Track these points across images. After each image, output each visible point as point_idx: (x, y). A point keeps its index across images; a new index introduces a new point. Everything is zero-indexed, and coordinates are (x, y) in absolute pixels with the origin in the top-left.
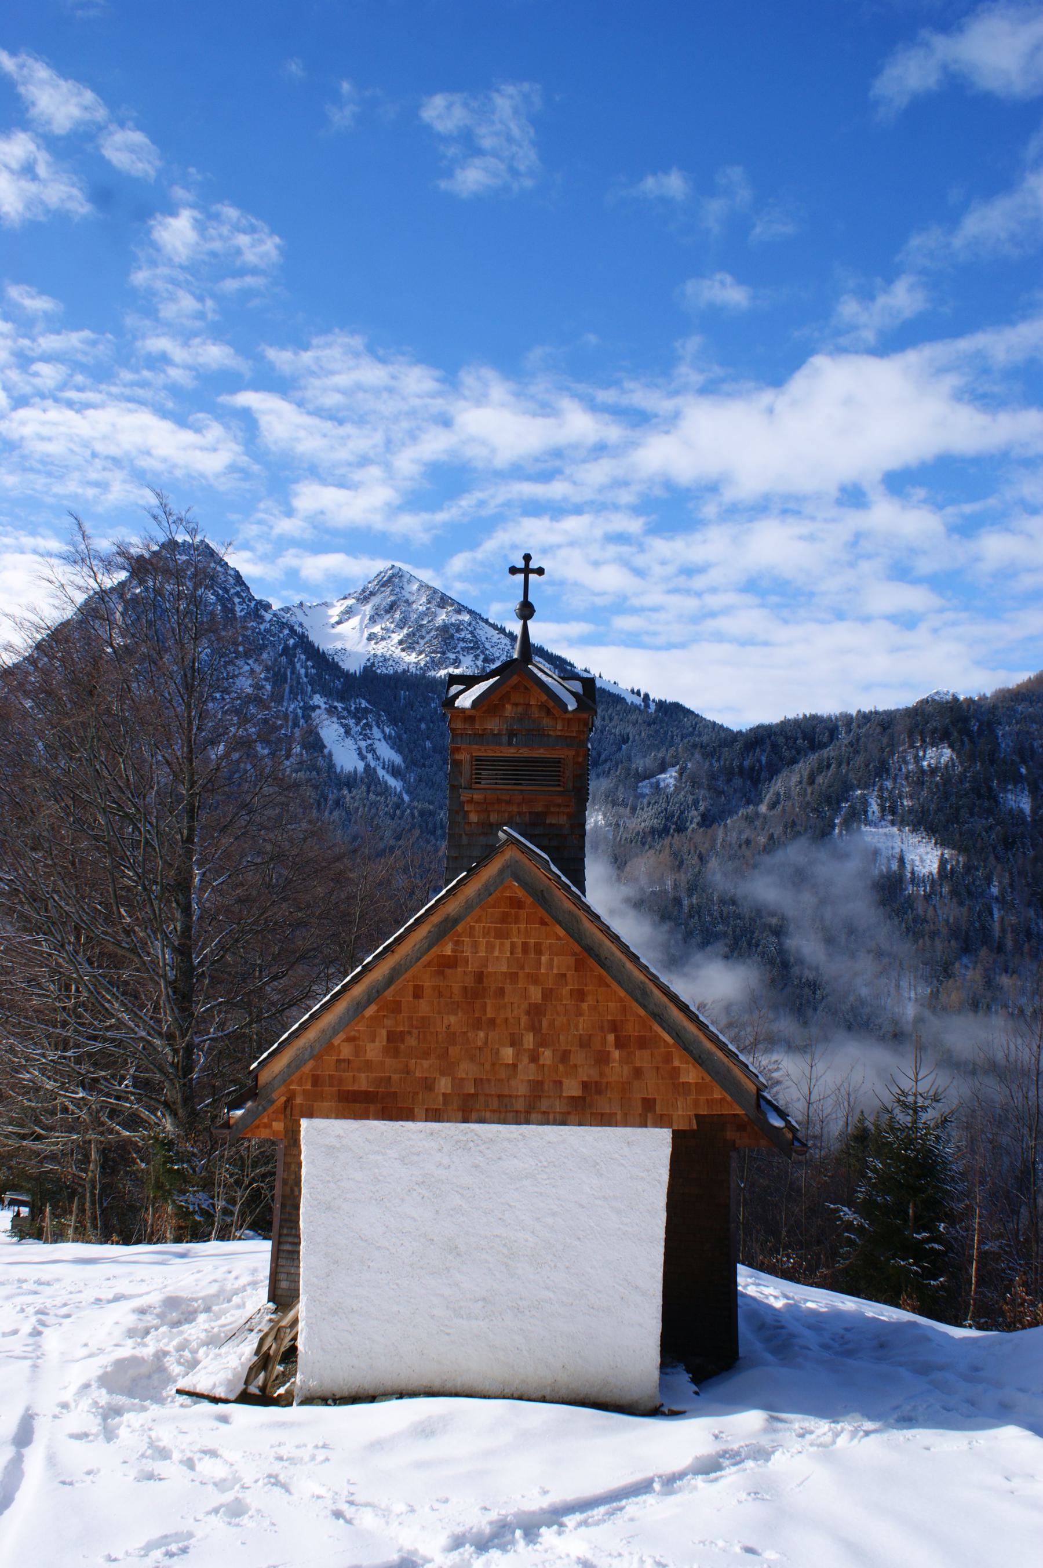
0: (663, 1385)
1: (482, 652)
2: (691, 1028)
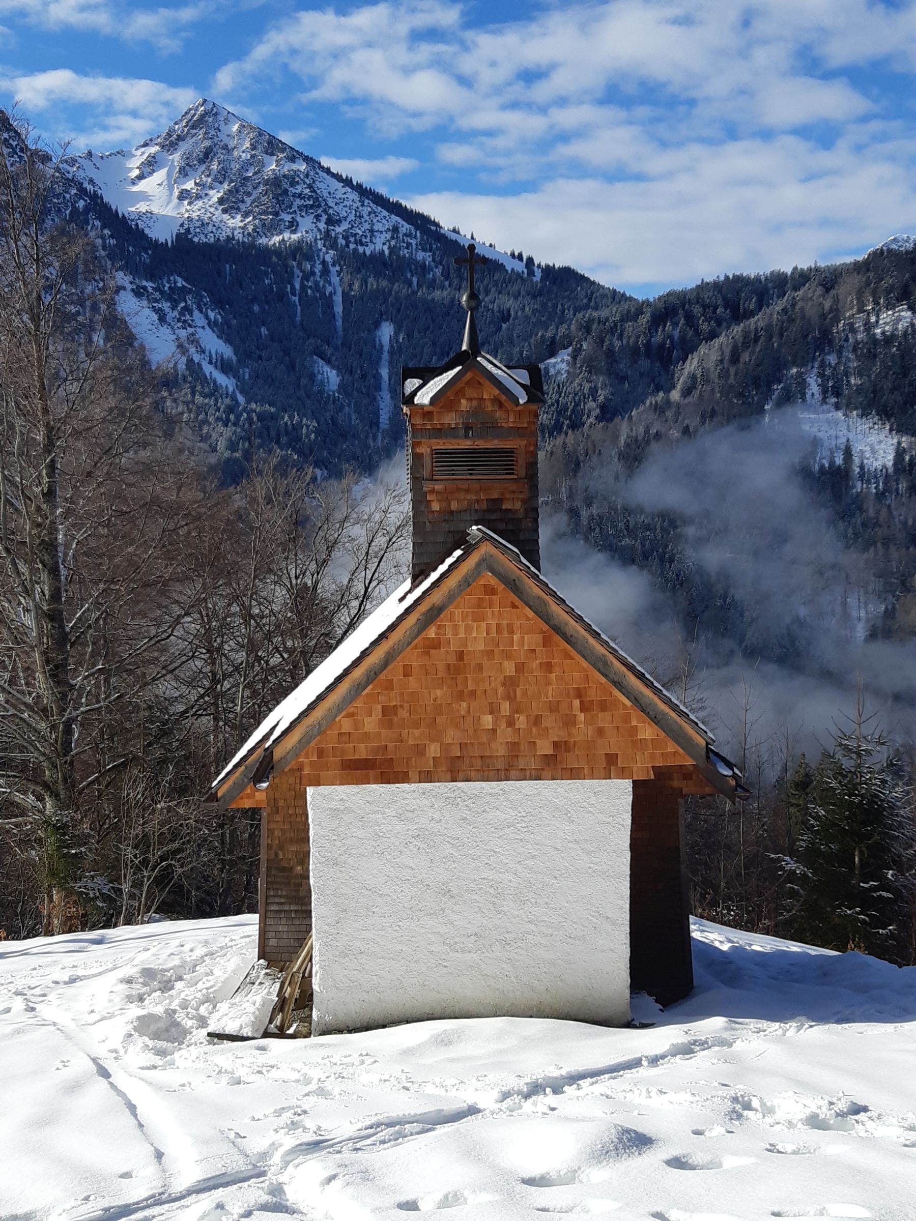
0: (632, 1005)
1: (325, 211)
2: (647, 692)
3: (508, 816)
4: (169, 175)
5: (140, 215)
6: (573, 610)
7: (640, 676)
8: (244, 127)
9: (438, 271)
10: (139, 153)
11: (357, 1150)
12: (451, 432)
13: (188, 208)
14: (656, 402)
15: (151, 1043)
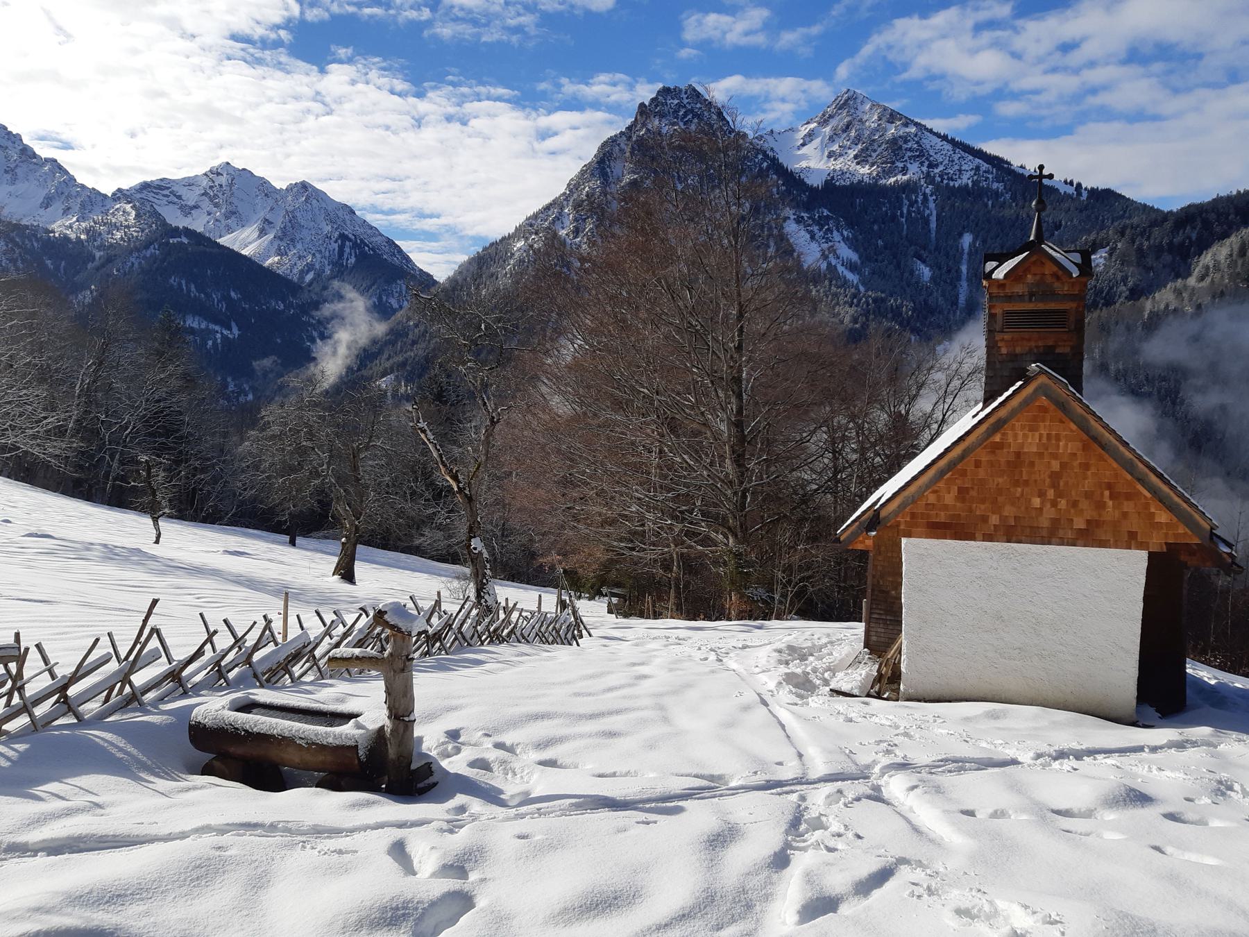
0: (1137, 711)
4: (822, 142)
5: (802, 170)
7: (1160, 476)
9: (1008, 196)
12: (1020, 298)
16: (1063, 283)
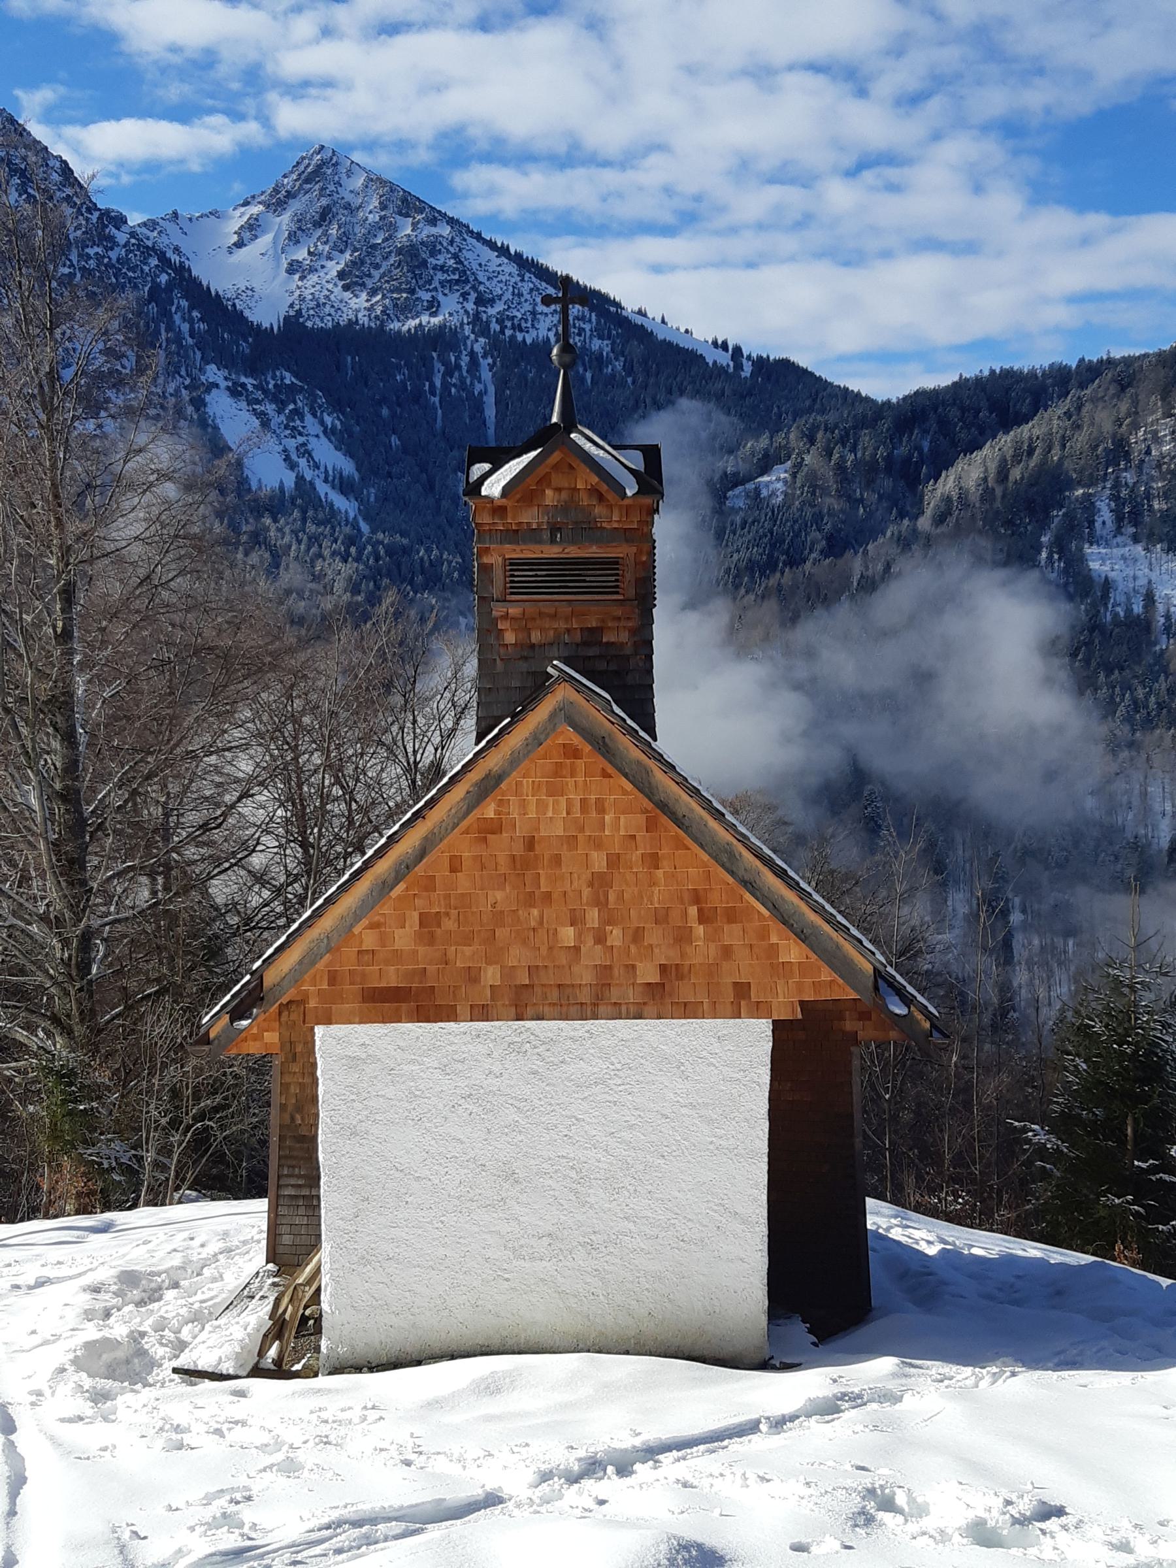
1: (474, 288)
2: (790, 896)
3: (596, 1069)
6: (686, 780)
7: (781, 874)
8: (372, 180)
9: (619, 365)
10: (238, 213)
11: (295, 1563)
13: (300, 283)
14: (900, 532)
15: (87, 1383)
16: (610, 507)
